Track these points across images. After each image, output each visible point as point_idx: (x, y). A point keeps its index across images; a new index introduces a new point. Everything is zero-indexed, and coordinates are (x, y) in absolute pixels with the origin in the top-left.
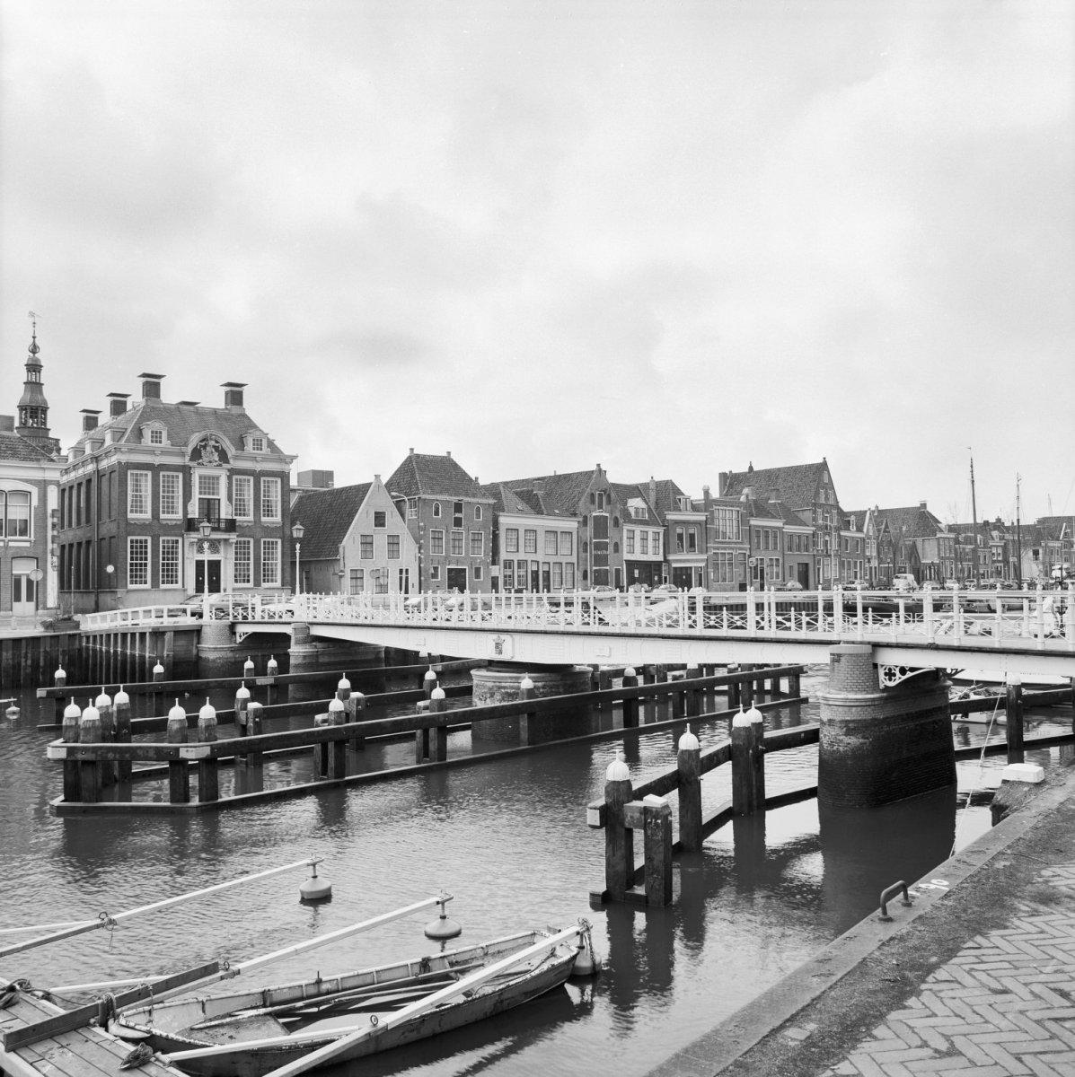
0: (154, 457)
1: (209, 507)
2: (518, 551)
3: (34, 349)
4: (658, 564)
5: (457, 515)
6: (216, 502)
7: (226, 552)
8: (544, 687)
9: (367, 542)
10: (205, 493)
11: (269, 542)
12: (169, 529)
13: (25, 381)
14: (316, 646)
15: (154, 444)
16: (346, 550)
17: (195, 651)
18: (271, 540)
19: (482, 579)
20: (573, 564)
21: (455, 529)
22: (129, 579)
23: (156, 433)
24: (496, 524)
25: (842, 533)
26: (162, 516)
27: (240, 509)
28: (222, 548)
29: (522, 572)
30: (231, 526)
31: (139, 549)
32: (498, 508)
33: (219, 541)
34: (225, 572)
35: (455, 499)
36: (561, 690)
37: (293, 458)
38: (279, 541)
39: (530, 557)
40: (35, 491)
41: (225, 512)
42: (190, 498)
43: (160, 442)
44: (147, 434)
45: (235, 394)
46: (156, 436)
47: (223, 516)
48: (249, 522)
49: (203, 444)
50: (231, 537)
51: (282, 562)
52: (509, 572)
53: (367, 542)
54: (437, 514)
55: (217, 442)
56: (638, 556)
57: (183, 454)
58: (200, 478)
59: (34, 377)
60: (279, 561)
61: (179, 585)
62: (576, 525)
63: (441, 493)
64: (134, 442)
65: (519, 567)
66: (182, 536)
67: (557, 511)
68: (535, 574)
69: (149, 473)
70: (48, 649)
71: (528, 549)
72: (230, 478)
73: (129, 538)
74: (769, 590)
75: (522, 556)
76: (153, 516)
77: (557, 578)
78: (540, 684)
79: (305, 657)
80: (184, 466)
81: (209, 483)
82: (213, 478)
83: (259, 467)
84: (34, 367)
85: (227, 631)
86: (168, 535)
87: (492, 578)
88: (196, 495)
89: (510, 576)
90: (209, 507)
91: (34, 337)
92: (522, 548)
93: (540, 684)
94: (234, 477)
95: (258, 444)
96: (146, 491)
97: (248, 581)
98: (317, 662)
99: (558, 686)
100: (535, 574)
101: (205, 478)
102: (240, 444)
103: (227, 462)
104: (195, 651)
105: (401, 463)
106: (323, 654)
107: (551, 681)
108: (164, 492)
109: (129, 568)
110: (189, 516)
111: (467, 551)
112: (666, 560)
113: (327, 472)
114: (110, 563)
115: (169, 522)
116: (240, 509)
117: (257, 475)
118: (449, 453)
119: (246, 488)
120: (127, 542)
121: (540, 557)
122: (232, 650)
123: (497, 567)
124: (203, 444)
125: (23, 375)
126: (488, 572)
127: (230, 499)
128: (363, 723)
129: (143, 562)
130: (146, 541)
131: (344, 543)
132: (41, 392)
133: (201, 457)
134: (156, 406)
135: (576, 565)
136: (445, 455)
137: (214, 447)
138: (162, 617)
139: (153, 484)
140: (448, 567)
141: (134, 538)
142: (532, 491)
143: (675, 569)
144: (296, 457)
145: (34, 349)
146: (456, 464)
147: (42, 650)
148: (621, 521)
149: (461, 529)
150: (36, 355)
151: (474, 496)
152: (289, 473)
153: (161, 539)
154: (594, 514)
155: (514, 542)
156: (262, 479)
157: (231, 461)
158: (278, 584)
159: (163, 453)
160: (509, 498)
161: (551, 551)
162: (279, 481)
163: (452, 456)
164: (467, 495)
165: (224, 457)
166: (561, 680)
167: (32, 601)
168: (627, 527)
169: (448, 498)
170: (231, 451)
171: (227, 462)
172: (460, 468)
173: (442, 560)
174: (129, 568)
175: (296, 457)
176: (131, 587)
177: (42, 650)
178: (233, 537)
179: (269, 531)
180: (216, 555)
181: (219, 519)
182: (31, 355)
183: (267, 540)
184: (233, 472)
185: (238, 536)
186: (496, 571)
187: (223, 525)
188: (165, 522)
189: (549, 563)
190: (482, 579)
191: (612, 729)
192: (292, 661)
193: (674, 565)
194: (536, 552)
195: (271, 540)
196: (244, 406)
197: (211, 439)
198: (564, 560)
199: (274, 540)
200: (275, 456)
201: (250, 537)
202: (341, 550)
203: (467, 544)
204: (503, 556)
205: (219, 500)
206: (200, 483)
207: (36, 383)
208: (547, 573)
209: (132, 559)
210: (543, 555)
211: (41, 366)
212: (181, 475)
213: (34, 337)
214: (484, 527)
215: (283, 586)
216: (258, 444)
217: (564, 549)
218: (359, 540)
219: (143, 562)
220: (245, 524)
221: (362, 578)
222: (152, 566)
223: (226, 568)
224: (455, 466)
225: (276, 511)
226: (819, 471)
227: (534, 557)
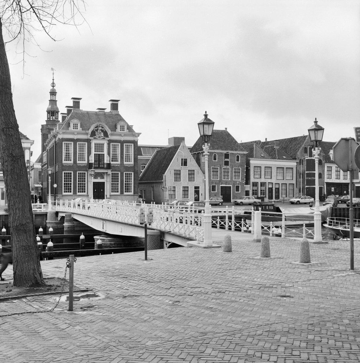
0: (74, 136)
1: (99, 158)
2: (261, 178)
3: (53, 85)
4: (347, 185)
5: (226, 160)
7: (107, 179)
8: (114, 244)
9: (177, 175)
10: (97, 152)
11: (128, 174)
12: (81, 168)
13: (50, 99)
14: (73, 223)
15: (74, 130)
16: (166, 177)
17: (45, 224)
18: (129, 173)
19: (240, 192)
20: (294, 184)
21: (225, 167)
22: (124, 190)
24: (248, 164)
25: (41, 186)
26: (78, 162)
27: (114, 159)
28: (105, 177)
29: (263, 188)
30: (109, 166)
31: (68, 176)
32: (251, 155)
33: (104, 173)
34: (107, 188)
35: (225, 152)
36: (122, 246)
37: (139, 134)
38: (133, 173)
39: (268, 181)
41: (106, 160)
42: (91, 154)
43: (77, 129)
44: (72, 125)
45: (115, 105)
46: (75, 126)
47: (105, 162)
48: (118, 164)
50: (109, 171)
51: (134, 183)
52: (255, 188)
53: (177, 175)
55: (102, 128)
56: (334, 180)
57: (87, 134)
58: (95, 144)
59: (53, 98)
60: (133, 182)
61: (85, 194)
62: (295, 164)
63: (218, 149)
64: (66, 129)
65: (261, 186)
66: (87, 171)
67: (284, 157)
68: (271, 190)
69: (72, 143)
70: (4, 221)
71: (267, 177)
72: (109, 144)
73: (63, 172)
74: (164, 204)
75: (263, 180)
76: (74, 162)
77: (284, 192)
78: (113, 243)
79: (68, 227)
80: (88, 139)
81: (99, 147)
82: (101, 144)
83: (122, 139)
84: (53, 93)
85: (55, 216)
86: (81, 171)
87: (246, 191)
88: (93, 152)
89: (256, 190)
90: (99, 158)
91: (53, 80)
92: (263, 176)
93: (113, 243)
94: (111, 144)
95: (122, 128)
96: (71, 151)
97: (118, 192)
98: (74, 230)
99: (121, 244)
100: (271, 190)
101: (97, 144)
102: (114, 128)
103: (108, 137)
104: (45, 224)
106: (77, 226)
107: (118, 241)
109: (77, 185)
110: (90, 162)
111: (232, 178)
112: (353, 184)
113: (181, 138)
114: (56, 183)
115: (81, 165)
116: (114, 159)
117: (122, 143)
118: (226, 128)
119: (130, 149)
120: (62, 174)
121: (274, 181)
122: (56, 223)
123: (249, 186)
125: (48, 97)
126: (243, 188)
127: (109, 154)
129: (84, 183)
130: (71, 173)
131: (165, 174)
132: (56, 104)
133: (95, 135)
134: (77, 112)
135: (295, 185)
136: (224, 129)
137: (101, 130)
138: (41, 208)
139: (74, 148)
140: (221, 185)
141: (66, 172)
142: (273, 147)
143: (356, 187)
144: (141, 133)
145: (53, 85)
146: (229, 134)
147: (1, 221)
148: (323, 162)
149: (228, 167)
150: (54, 87)
151: (236, 150)
152: (137, 141)
153: (78, 172)
154: (306, 158)
155: (259, 173)
157: (109, 136)
158: (132, 193)
159: (78, 133)
160: (257, 150)
161: (281, 178)
162: (133, 145)
163: (228, 130)
164: (232, 150)
165: (106, 134)
166: (122, 241)
167: (4, 199)
168: (326, 165)
169: (221, 151)
170: (109, 132)
171: (108, 137)
172: (231, 136)
173: (217, 182)
174: (77, 185)
175: (141, 133)
176: (64, 194)
177: (1, 221)
178: (109, 172)
179: (128, 168)
180: (102, 180)
181: (104, 163)
182: (52, 87)
183: (127, 172)
184: (110, 141)
185: (111, 171)
186: (249, 188)
187: (105, 166)
188: (79, 165)
189: (279, 184)
190: (240, 192)
192: (65, 229)
193: (356, 185)
194: (271, 178)
195: (129, 173)
196: (119, 110)
197: (100, 127)
198: (288, 182)
199: (130, 173)
200: (130, 133)
201: (118, 171)
202: (164, 177)
203: (232, 174)
204: (252, 180)
205: (104, 154)
206: (95, 147)
207: (54, 100)
208: (277, 190)
209: (79, 181)
210: (275, 179)
211: (57, 93)
212: (86, 143)
213: (53, 80)
214: (241, 165)
215: (134, 194)
216: (122, 128)
217: (288, 176)
218: (173, 172)
219: (84, 183)
220: (116, 165)
221: (188, 191)
222: (121, 184)
223: (107, 184)
224: (229, 135)
225: (132, 159)
227: (269, 181)
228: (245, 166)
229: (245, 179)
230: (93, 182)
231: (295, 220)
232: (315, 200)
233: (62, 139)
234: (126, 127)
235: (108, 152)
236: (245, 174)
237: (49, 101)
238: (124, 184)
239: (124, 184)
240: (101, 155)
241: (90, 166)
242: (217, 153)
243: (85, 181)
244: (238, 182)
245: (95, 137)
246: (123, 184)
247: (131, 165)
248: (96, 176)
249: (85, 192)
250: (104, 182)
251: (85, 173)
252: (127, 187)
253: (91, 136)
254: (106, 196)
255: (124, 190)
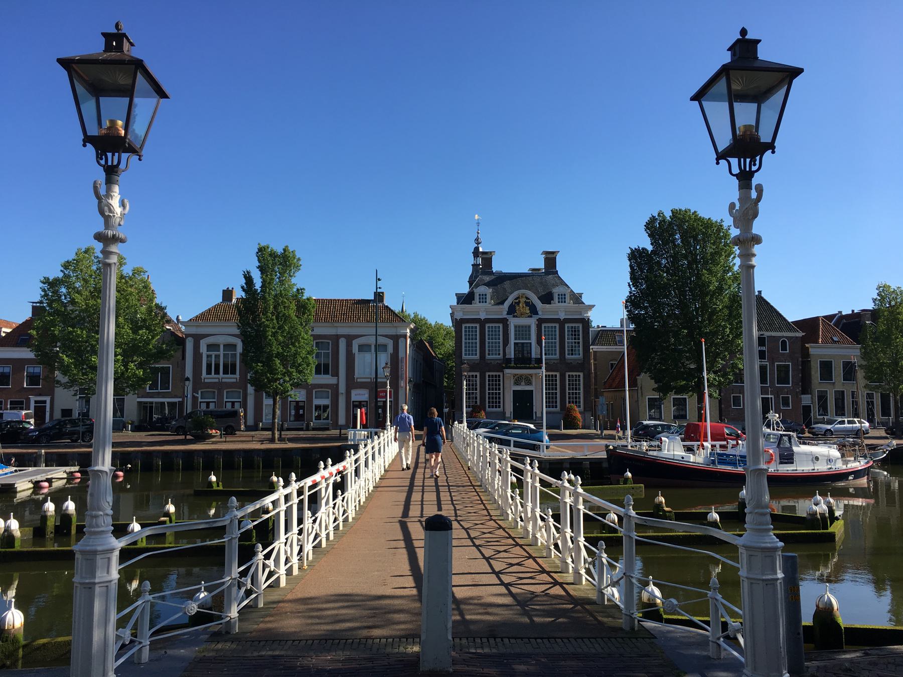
6: (529, 345)
22: (487, 404)
23: (483, 295)
26: (487, 357)
40: (390, 343)
49: (517, 301)
54: (784, 348)
58: (515, 327)
81: (523, 331)
82: (526, 326)
91: (478, 233)
101: (519, 326)
105: (774, 306)
108: (489, 339)
110: (507, 357)
124: (517, 301)
128: (816, 531)
141: (491, 374)
156: (487, 325)
165: (534, 311)
170: (539, 305)
174: (487, 396)
191: (165, 544)
206: (530, 335)
226: (223, 290)
228: (800, 359)
229: (800, 384)
230: (513, 391)
231: (286, 521)
232: (243, 431)
233: (461, 319)
234: (568, 297)
235: (537, 341)
236: (800, 375)
237: (472, 265)
238: (567, 394)
239: (567, 394)
240: (525, 345)
241: (506, 363)
242: (786, 337)
243: (499, 390)
244: (786, 390)
245: (516, 314)
246: (565, 393)
247: (579, 360)
248: (518, 380)
249: (499, 407)
250: (532, 391)
251: (499, 376)
252: (553, 401)
253: (508, 314)
254: (536, 413)
255: (487, 404)
